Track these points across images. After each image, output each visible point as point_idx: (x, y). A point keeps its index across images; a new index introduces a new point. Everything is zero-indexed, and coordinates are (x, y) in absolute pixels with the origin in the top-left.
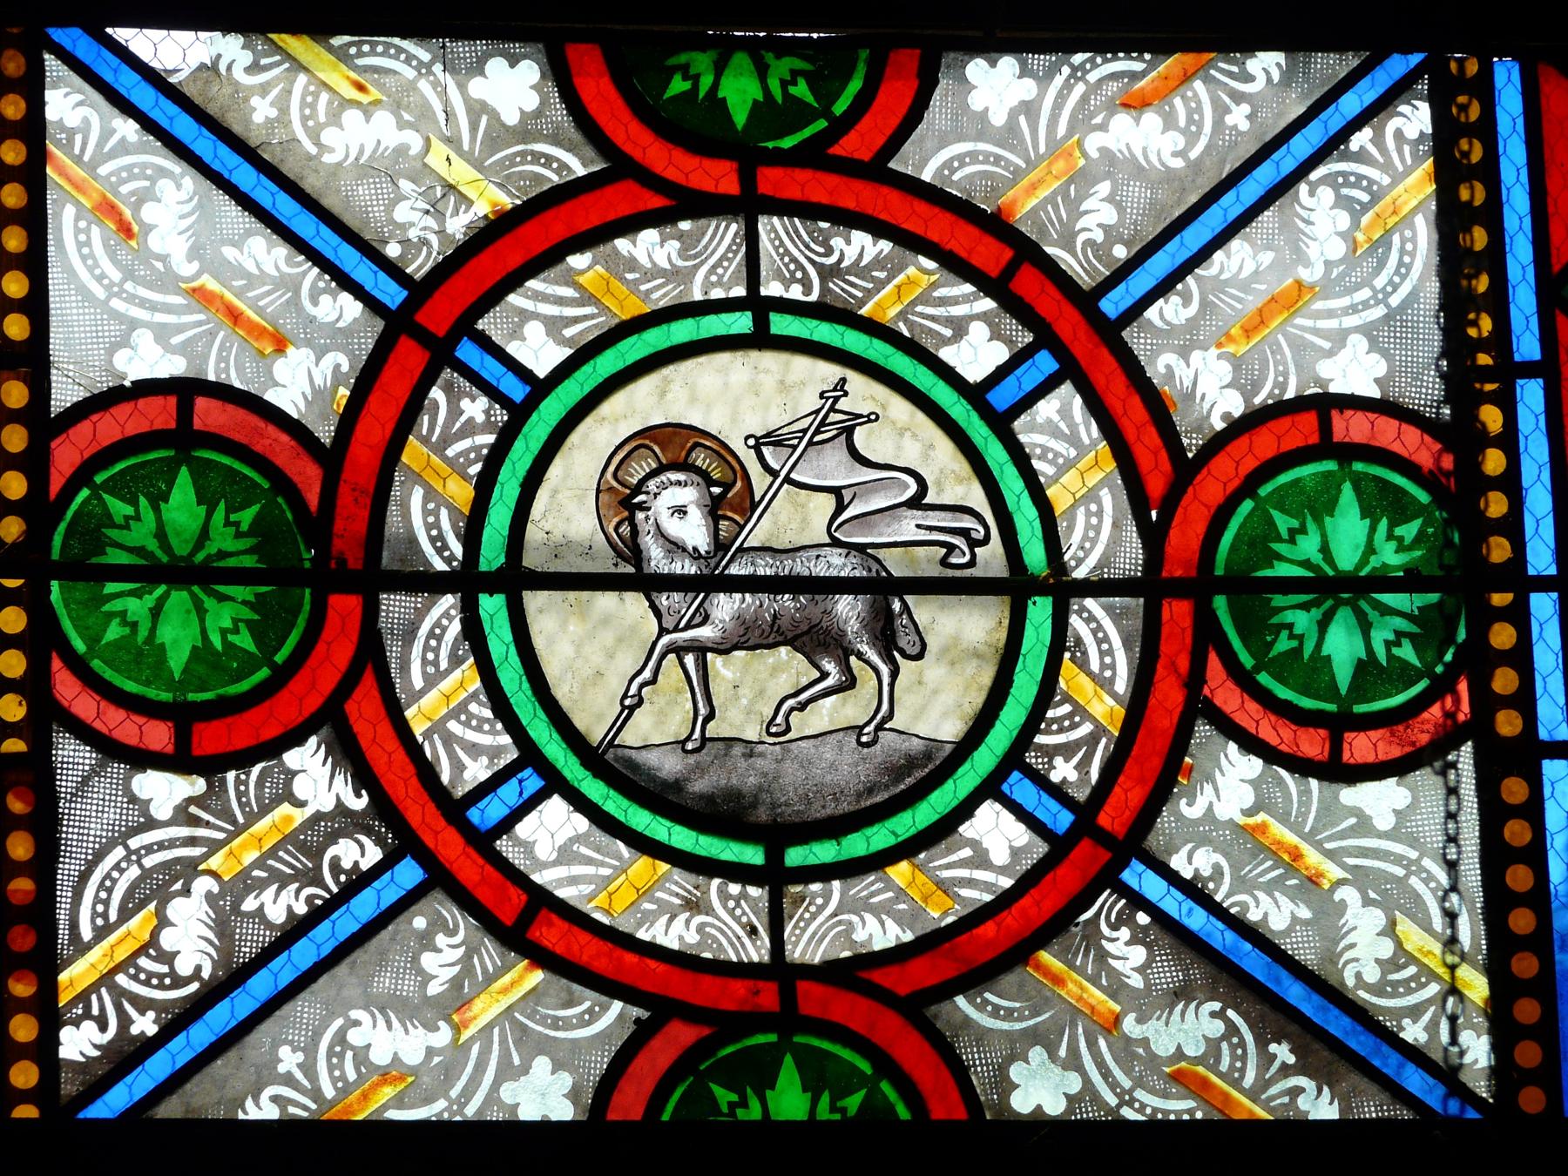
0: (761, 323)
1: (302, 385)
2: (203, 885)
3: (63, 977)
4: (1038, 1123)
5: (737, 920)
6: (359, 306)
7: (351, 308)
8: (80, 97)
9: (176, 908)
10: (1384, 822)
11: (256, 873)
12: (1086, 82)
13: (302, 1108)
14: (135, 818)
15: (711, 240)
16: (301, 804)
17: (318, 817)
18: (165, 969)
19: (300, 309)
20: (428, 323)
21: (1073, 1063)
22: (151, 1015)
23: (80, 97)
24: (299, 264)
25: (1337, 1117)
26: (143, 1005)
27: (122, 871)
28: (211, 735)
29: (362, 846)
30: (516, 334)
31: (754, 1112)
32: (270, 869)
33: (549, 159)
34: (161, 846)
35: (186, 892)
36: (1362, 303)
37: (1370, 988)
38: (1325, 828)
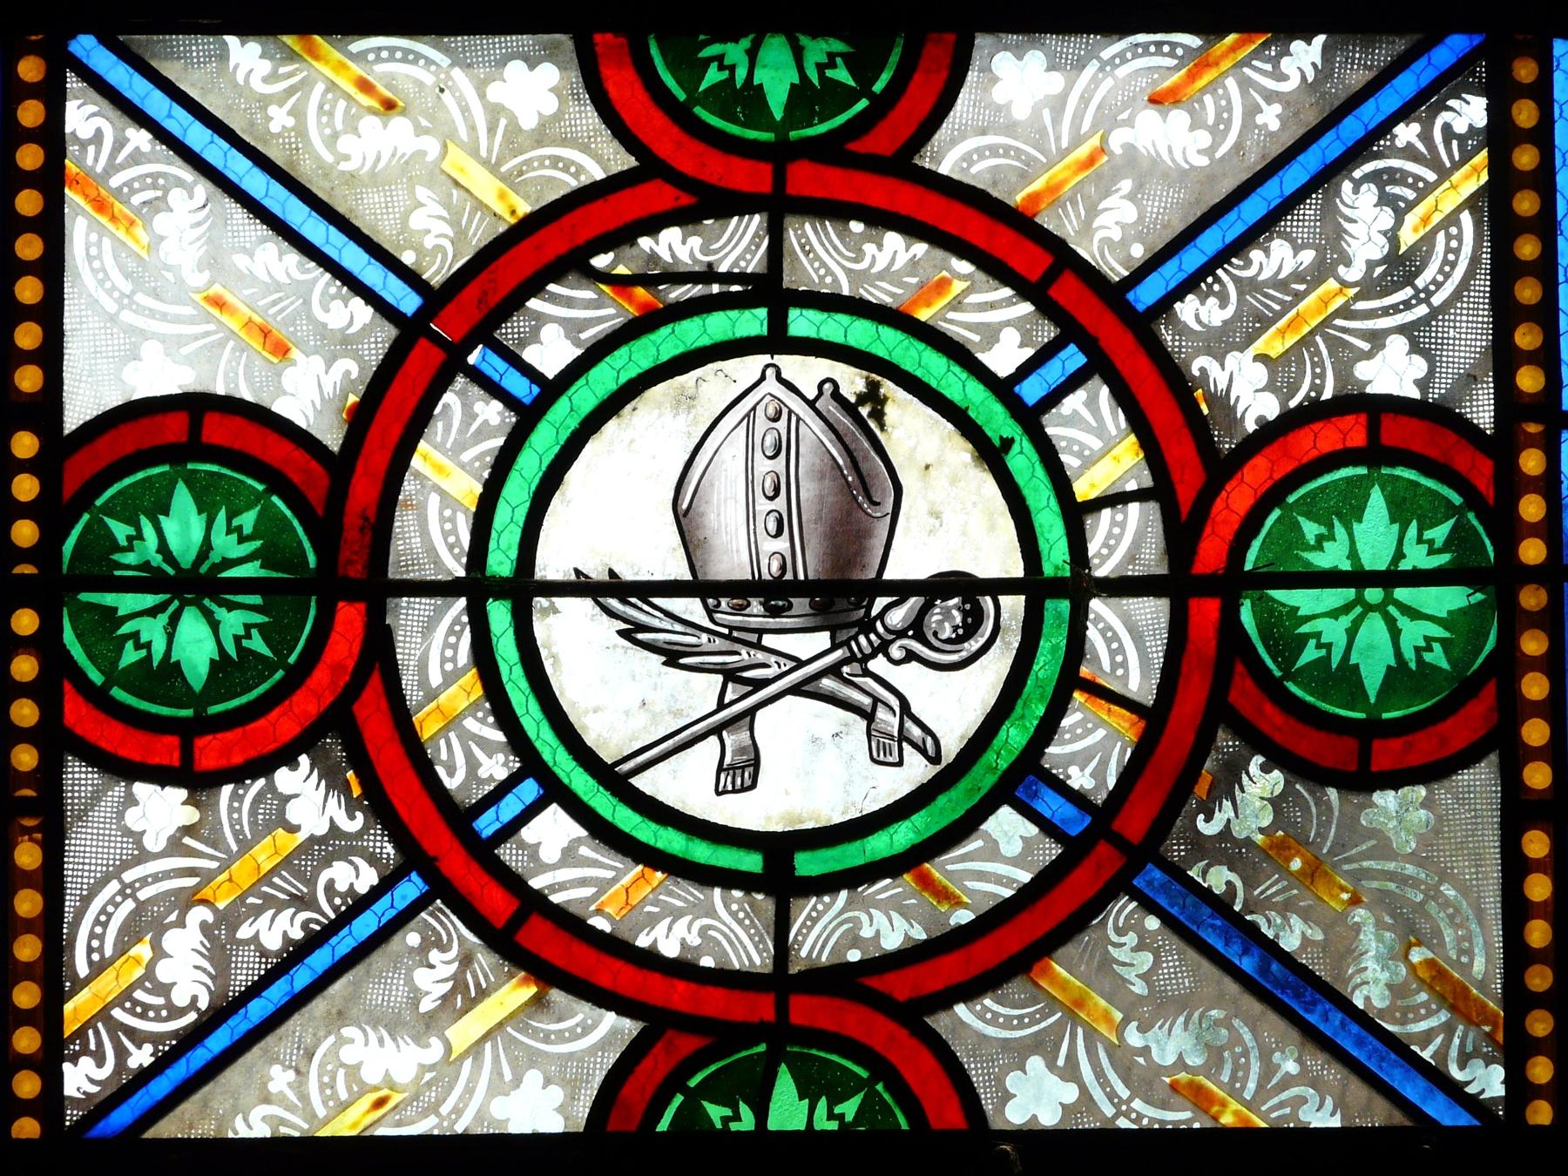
0: (778, 322)
1: (312, 394)
2: (1354, 273)
3: (68, 1008)
4: (1032, 1139)
5: (823, 264)
6: (370, 310)
7: (362, 312)
8: (95, 109)
9: (171, 940)
10: (151, 349)
11: (251, 900)
12: (1114, 77)
13: (295, 1126)
14: (129, 849)
15: (833, 931)
16: (1262, 358)
17: (312, 839)
18: (160, 1001)
19: (311, 318)
20: (443, 330)
21: (1070, 1073)
22: (1400, 143)
23: (95, 109)
24: (308, 271)
25: (1338, 1125)
26: (1409, 153)
27: (117, 906)
28: (200, 745)
29: (357, 869)
30: (534, 337)
31: (747, 1122)
32: (1287, 291)
33: (993, 1022)
34: (157, 878)
35: (180, 923)
36: (1403, 302)
37: (180, 183)
38: (212, 345)
